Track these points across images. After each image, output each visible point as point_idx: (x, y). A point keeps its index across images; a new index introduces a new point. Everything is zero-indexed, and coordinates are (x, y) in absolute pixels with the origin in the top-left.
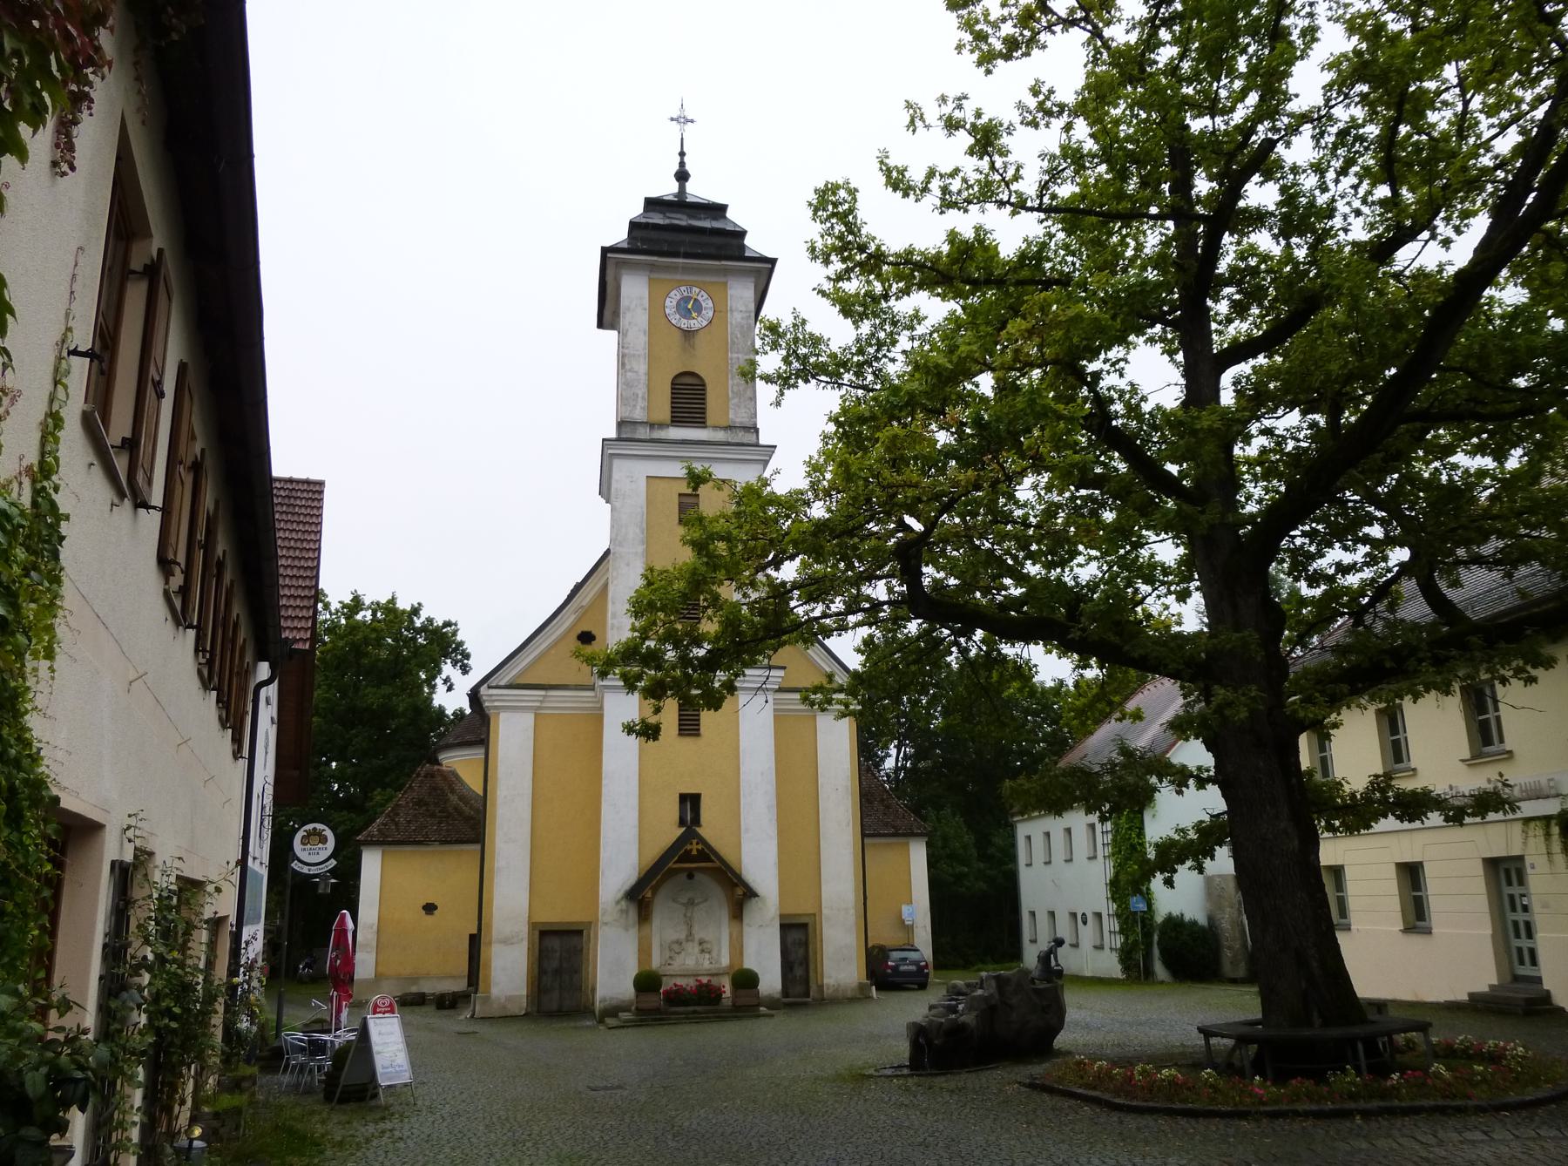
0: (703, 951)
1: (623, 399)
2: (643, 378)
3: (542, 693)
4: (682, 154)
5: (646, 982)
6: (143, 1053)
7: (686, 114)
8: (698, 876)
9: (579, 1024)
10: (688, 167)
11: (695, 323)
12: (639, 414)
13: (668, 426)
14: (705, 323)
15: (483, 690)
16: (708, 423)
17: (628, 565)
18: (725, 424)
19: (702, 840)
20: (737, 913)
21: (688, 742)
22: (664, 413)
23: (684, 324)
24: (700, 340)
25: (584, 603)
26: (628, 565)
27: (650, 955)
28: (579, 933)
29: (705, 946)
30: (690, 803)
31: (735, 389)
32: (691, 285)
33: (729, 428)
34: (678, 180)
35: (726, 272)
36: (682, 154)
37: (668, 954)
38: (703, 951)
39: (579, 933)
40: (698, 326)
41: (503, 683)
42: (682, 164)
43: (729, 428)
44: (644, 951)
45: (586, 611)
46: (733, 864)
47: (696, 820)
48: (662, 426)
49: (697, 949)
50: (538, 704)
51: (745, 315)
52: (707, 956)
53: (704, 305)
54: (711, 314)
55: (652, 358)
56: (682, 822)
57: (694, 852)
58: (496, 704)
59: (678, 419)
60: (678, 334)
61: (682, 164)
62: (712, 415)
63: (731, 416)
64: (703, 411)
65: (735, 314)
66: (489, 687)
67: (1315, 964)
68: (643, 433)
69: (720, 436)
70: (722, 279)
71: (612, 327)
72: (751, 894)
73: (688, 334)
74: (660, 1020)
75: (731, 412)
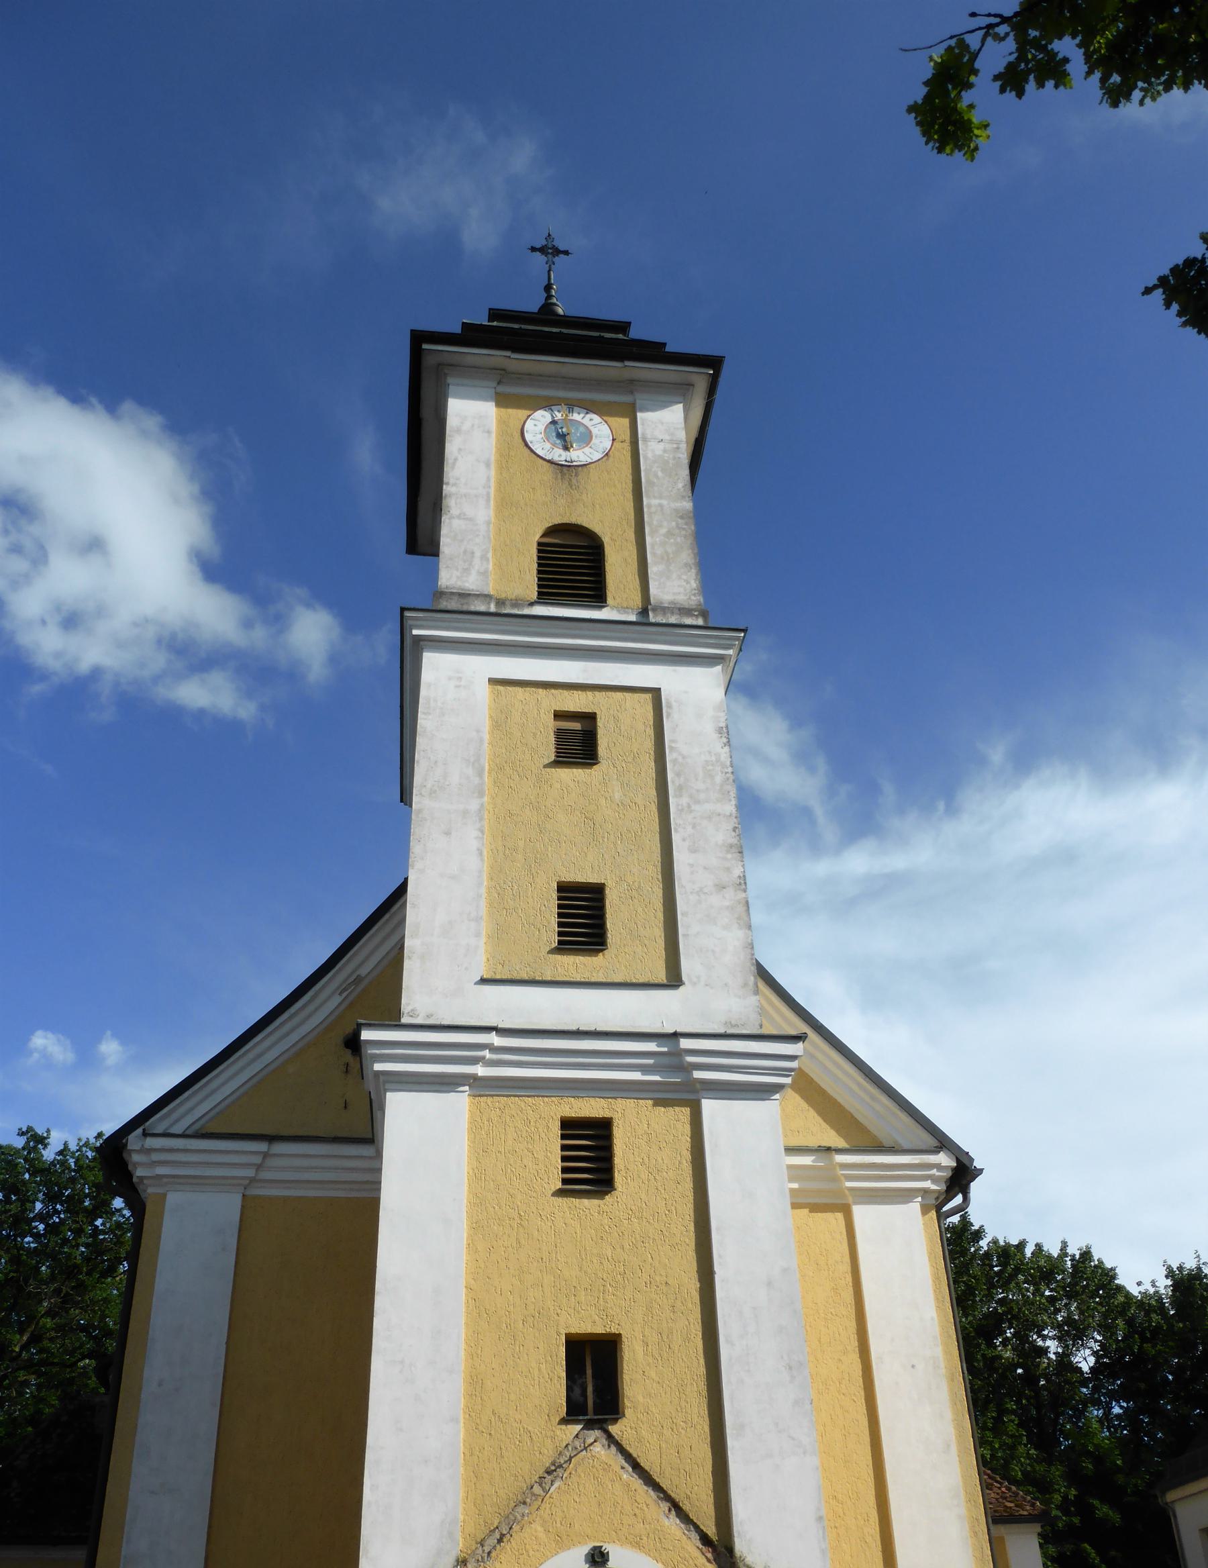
3: (262, 1146)
6: (957, 1233)
7: (556, 243)
11: (579, 455)
15: (134, 1140)
17: (448, 833)
21: (591, 1324)
23: (559, 455)
25: (363, 971)
26: (448, 833)
30: (1085, 79)
31: (659, 551)
32: (571, 406)
35: (630, 386)
41: (177, 1129)
50: (250, 1173)
51: (669, 446)
53: (594, 431)
55: (505, 503)
58: (161, 1171)
59: (549, 590)
60: (547, 472)
67: (1088, 1547)
70: (627, 399)
73: (566, 470)
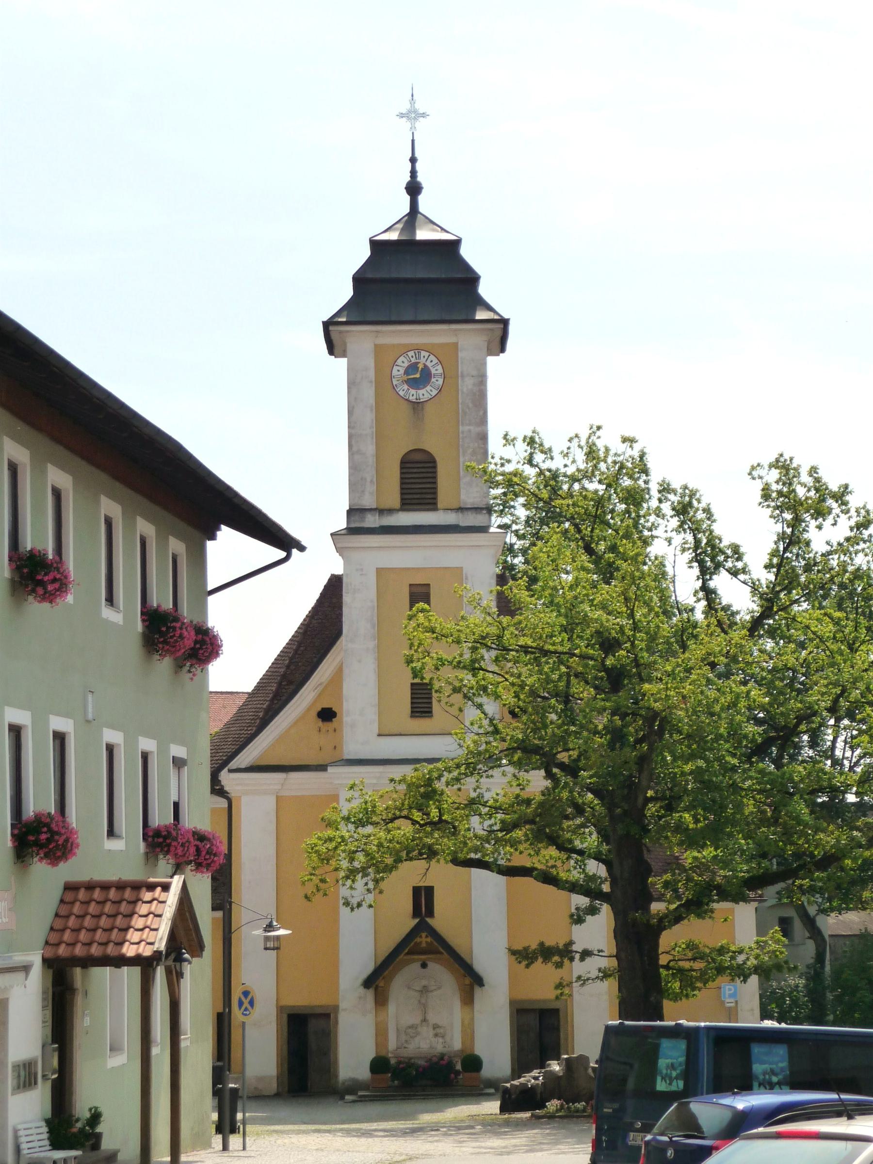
0: (436, 1035)
1: (354, 486)
2: (371, 460)
4: (413, 160)
5: (379, 1065)
7: (409, 125)
8: (431, 965)
9: (427, 1118)
10: (420, 178)
12: (368, 501)
13: (398, 510)
14: (434, 392)
16: (440, 506)
17: (360, 661)
18: (456, 506)
19: (434, 933)
20: (468, 999)
22: (394, 499)
23: (413, 394)
24: (429, 409)
26: (360, 661)
27: (386, 1039)
28: (327, 1016)
29: (438, 1031)
33: (461, 509)
34: (408, 193)
36: (413, 160)
37: (403, 1037)
38: (436, 1035)
39: (327, 1016)
40: (427, 396)
42: (413, 173)
43: (461, 509)
44: (381, 1033)
45: (326, 687)
46: (469, 962)
47: (430, 913)
48: (391, 511)
49: (431, 1033)
52: (441, 1040)
54: (441, 381)
55: (380, 437)
56: (416, 912)
57: (424, 945)
59: (409, 502)
61: (413, 173)
62: (443, 498)
63: (463, 497)
64: (434, 491)
65: (467, 379)
66: (230, 771)
68: (372, 521)
69: (450, 518)
71: (343, 355)
72: (478, 980)
73: (417, 406)
74: (409, 1095)
75: (463, 492)
